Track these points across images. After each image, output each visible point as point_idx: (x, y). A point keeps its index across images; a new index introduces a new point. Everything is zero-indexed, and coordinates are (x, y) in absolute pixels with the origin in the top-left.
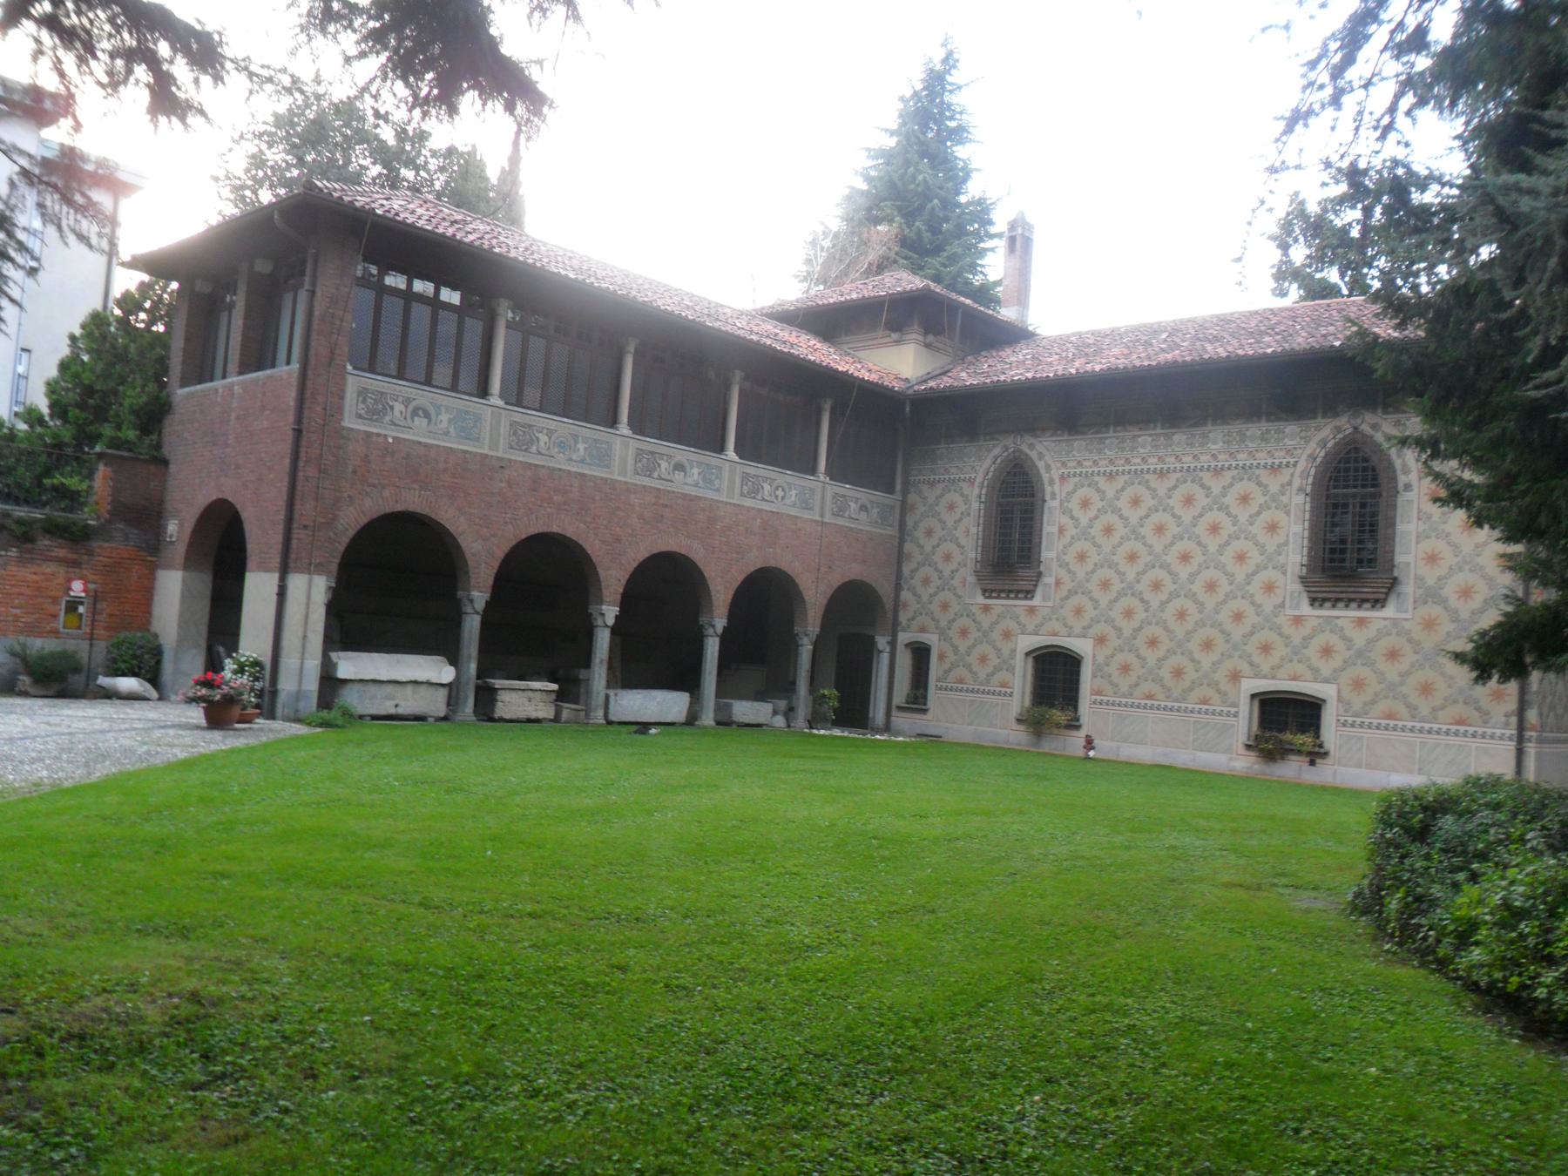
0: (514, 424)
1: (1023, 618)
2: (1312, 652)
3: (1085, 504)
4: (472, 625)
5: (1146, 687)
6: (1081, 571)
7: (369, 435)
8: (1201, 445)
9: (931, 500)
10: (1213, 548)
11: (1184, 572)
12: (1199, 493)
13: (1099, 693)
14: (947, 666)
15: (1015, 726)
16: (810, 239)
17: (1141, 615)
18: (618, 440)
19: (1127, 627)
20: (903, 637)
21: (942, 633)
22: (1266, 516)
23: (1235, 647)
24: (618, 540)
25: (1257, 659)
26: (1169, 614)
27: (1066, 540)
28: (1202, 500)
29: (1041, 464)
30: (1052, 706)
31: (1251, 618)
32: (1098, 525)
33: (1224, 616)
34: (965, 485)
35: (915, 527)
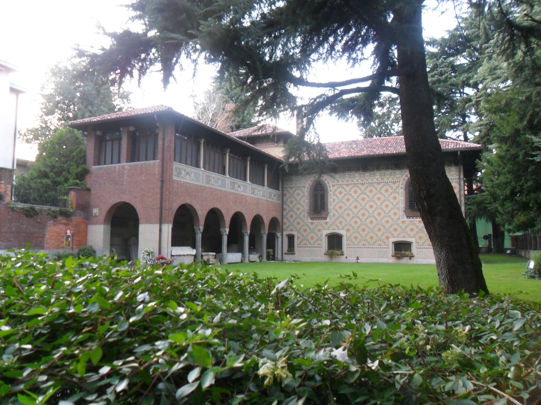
0: (207, 176)
1: (324, 225)
2: (408, 230)
4: (199, 237)
5: (363, 242)
6: (341, 212)
7: (178, 181)
8: (374, 176)
10: (379, 204)
11: (371, 211)
13: (349, 245)
15: (324, 256)
16: (131, 97)
17: (359, 223)
19: (356, 227)
20: (285, 233)
21: (298, 231)
22: (393, 195)
23: (387, 230)
25: (393, 233)
27: (336, 203)
28: (359, 192)
29: (326, 182)
31: (391, 222)
32: (345, 198)
33: (383, 222)
34: (303, 189)
35: (287, 200)
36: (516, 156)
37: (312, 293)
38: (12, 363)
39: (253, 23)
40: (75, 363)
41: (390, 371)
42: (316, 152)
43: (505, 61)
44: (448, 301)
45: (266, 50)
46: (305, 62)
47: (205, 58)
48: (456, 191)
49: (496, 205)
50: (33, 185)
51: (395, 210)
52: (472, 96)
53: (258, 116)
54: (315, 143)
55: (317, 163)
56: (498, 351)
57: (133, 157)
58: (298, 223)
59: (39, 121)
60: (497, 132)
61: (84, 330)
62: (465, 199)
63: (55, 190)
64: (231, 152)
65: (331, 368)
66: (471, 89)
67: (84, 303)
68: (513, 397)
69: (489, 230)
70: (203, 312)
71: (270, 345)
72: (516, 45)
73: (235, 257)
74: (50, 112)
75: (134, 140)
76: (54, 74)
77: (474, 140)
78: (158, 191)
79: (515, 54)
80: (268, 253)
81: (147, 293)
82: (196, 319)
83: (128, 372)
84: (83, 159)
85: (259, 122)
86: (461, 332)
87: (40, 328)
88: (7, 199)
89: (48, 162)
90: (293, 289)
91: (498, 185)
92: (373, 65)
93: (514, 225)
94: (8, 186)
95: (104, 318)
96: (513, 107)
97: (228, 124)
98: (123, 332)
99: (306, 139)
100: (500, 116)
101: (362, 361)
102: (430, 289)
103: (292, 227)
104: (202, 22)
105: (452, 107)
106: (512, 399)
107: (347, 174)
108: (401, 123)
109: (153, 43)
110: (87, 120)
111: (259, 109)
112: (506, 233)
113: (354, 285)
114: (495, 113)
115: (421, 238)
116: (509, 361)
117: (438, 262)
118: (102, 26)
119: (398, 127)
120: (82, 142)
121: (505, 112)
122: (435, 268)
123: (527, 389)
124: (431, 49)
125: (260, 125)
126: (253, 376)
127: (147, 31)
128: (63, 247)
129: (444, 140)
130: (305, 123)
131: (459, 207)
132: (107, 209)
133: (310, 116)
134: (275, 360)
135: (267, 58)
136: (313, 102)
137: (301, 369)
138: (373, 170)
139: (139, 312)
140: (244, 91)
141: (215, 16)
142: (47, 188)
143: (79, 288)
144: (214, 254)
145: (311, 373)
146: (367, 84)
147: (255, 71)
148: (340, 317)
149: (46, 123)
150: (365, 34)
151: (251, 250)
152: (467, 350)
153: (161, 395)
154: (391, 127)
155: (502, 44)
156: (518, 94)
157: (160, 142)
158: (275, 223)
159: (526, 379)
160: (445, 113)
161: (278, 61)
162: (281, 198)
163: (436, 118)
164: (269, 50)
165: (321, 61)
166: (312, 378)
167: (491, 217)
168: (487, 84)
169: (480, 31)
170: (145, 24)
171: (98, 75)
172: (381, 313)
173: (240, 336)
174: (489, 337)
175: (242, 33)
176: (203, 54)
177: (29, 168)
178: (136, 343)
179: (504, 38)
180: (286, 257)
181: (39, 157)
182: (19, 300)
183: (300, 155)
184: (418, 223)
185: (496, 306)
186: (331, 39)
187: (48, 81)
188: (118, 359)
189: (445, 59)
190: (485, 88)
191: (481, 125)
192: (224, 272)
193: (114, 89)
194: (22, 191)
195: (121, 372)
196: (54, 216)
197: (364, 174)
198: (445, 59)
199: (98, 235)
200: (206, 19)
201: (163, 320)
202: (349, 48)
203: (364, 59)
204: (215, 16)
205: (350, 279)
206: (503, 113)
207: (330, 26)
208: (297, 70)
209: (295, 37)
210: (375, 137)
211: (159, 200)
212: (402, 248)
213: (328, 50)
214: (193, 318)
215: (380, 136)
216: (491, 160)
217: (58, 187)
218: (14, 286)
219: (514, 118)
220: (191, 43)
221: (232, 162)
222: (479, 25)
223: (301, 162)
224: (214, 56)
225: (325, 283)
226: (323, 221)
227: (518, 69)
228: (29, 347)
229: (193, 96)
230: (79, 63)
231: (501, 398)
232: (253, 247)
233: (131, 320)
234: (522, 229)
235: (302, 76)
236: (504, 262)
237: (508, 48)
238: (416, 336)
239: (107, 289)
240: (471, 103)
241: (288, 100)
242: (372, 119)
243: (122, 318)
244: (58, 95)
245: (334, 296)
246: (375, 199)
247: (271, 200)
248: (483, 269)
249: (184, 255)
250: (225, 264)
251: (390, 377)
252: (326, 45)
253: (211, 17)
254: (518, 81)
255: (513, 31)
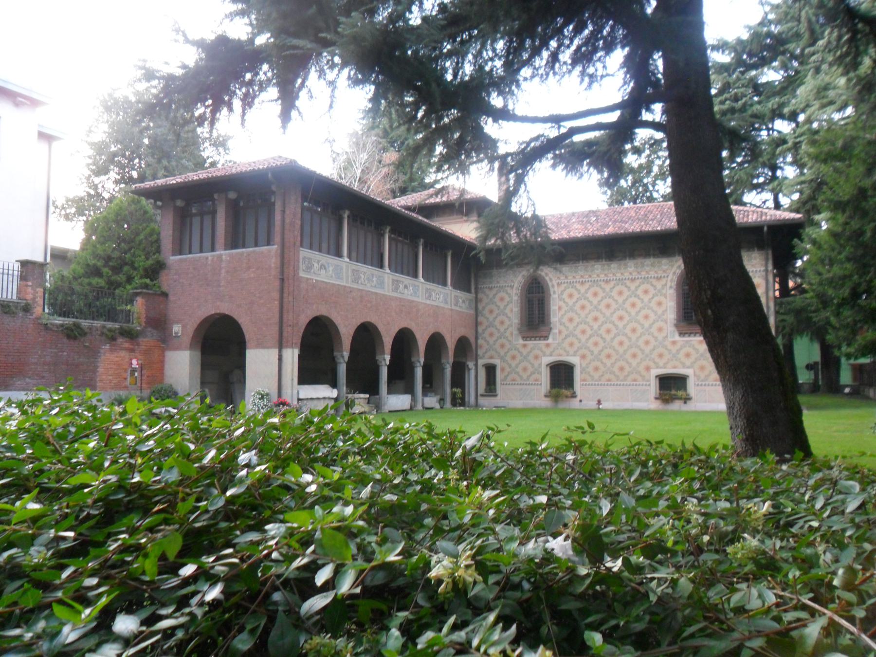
0: (353, 270)
1: (544, 349)
2: (681, 355)
3: (571, 296)
4: (342, 369)
5: (607, 376)
6: (571, 327)
7: (308, 279)
9: (491, 296)
10: (633, 314)
11: (620, 324)
12: (625, 290)
13: (584, 380)
14: (506, 373)
15: (544, 398)
16: (230, 144)
18: (386, 275)
19: (596, 351)
20: (481, 362)
21: (502, 359)
22: (656, 299)
23: (647, 356)
24: (389, 324)
25: (657, 360)
26: (615, 343)
27: (563, 312)
28: (601, 294)
29: (547, 278)
30: (561, 388)
31: (653, 343)
33: (641, 343)
35: (484, 308)
36: (860, 233)
37: (522, 455)
38: (44, 559)
39: (425, 19)
40: (140, 558)
41: (640, 574)
42: (530, 230)
43: (842, 75)
44: (742, 467)
45: (448, 64)
46: (512, 83)
47: (349, 78)
48: (760, 291)
49: (827, 314)
50: (77, 288)
51: (660, 324)
52: (787, 135)
53: (435, 172)
54: (529, 215)
55: (532, 247)
56: (820, 545)
57: (235, 241)
58: (502, 346)
59: (85, 184)
60: (829, 193)
61: (156, 509)
62: (776, 305)
63: (113, 295)
64: (392, 232)
65: (547, 569)
66: (786, 122)
67: (155, 468)
68: (842, 617)
69: (816, 356)
70: (343, 481)
71: (451, 534)
72: (862, 48)
73: (400, 401)
74: (102, 171)
75: (236, 213)
76: (108, 109)
77: (790, 207)
78: (276, 295)
79: (860, 63)
80: (454, 395)
81: (254, 452)
82: (332, 494)
83: (223, 572)
84: (155, 246)
85: (436, 182)
86: (755, 512)
87: (88, 507)
88: (38, 310)
89: (100, 250)
90: (490, 448)
91: (831, 281)
92: (623, 86)
93: (856, 346)
94: (38, 290)
95: (188, 490)
96: (856, 152)
97: (388, 186)
98: (217, 512)
99: (514, 208)
100: (833, 166)
101: (596, 560)
102: (713, 448)
103: (492, 353)
104: (342, 19)
105: (755, 153)
106: (837, 618)
107: (581, 265)
108: (669, 180)
109: (264, 55)
110: (160, 182)
111: (436, 160)
112: (843, 360)
113: (589, 442)
114: (825, 161)
115: (702, 368)
116: (837, 561)
117: (730, 408)
118: (182, 29)
119: (664, 187)
120: (154, 218)
121: (842, 159)
122: (725, 418)
123: (864, 603)
124: (718, 58)
125: (438, 186)
126: (422, 582)
127: (255, 35)
128: (126, 387)
129: (741, 208)
130: (512, 182)
131: (764, 319)
132: (195, 326)
133: (520, 171)
134: (456, 556)
135: (449, 77)
136: (525, 148)
137: (499, 572)
138: (624, 258)
139: (241, 481)
140: (412, 132)
141: (364, 8)
142: (99, 293)
143: (148, 446)
144: (367, 396)
145: (516, 579)
146: (613, 117)
147: (432, 100)
148: (566, 492)
149: (95, 187)
150: (609, 34)
151: (426, 391)
152: (769, 543)
153: (277, 610)
154: (653, 186)
155: (837, 47)
156: (864, 128)
157: (278, 217)
158: (464, 346)
159: (863, 587)
160: (742, 163)
161: (466, 82)
162: (474, 305)
163: (727, 172)
164: (451, 64)
165: (537, 79)
166: (518, 587)
167: (819, 334)
168: (813, 113)
169: (801, 26)
170: (251, 24)
171: (177, 109)
172: (631, 485)
173: (404, 522)
174: (806, 522)
175: (408, 36)
176: (346, 71)
177: (70, 261)
178: (238, 529)
179: (840, 37)
180: (481, 401)
181: (86, 243)
182: (55, 464)
183: (503, 234)
184: (698, 344)
185: (820, 475)
186: (553, 44)
187: (97, 120)
188: (209, 554)
189: (743, 73)
190: (809, 121)
191: (802, 183)
192: (380, 423)
193: (203, 131)
194: (60, 297)
195: (212, 572)
196: (111, 338)
197: (609, 265)
198: (743, 73)
199: (182, 366)
200: (348, 14)
201: (279, 494)
202: (582, 58)
203: (608, 75)
204: (364, 8)
205: (583, 433)
206: (840, 161)
207: (552, 22)
208: (498, 95)
209: (494, 41)
210: (626, 204)
211: (277, 309)
212: (671, 386)
213: (548, 62)
214: (326, 492)
215: (635, 203)
216: (818, 240)
217: (117, 291)
218: (48, 443)
219: (857, 169)
220: (325, 54)
221: (394, 247)
222: (799, 15)
223: (506, 246)
224: (363, 75)
225: (543, 438)
226: (542, 343)
227: (863, 88)
228: (71, 534)
229: (330, 141)
230: (146, 90)
231: (820, 616)
232: (429, 385)
233: (229, 493)
234: (869, 353)
235: (506, 106)
236: (838, 407)
237: (847, 54)
238: (688, 522)
239: (192, 447)
240: (785, 146)
241: (484, 145)
242: (622, 174)
243: (216, 492)
244: (113, 143)
245: (556, 459)
246: (627, 305)
247: (458, 309)
248: (804, 418)
249: (318, 399)
250: (385, 413)
251: (641, 583)
252: (545, 54)
253: (356, 10)
254: (865, 107)
255: (856, 25)
